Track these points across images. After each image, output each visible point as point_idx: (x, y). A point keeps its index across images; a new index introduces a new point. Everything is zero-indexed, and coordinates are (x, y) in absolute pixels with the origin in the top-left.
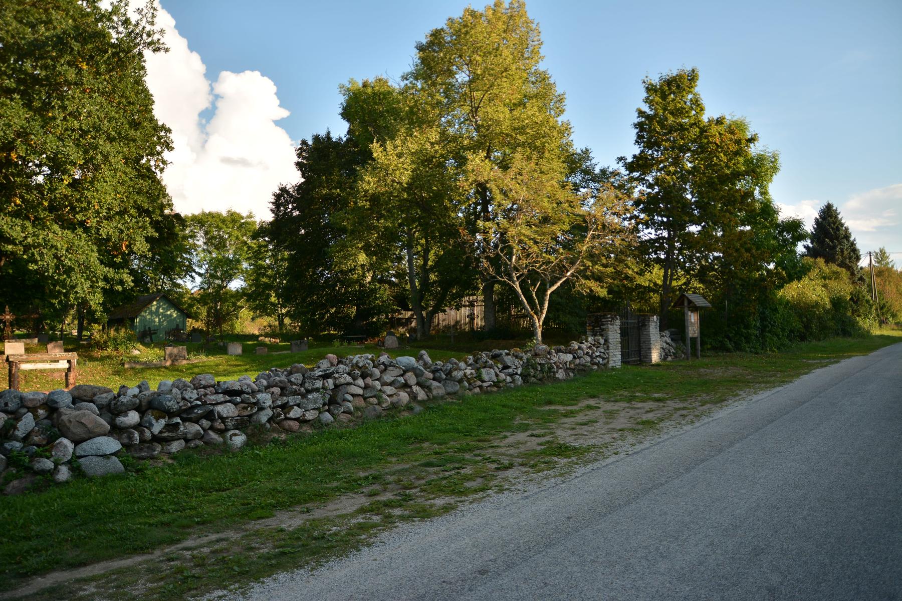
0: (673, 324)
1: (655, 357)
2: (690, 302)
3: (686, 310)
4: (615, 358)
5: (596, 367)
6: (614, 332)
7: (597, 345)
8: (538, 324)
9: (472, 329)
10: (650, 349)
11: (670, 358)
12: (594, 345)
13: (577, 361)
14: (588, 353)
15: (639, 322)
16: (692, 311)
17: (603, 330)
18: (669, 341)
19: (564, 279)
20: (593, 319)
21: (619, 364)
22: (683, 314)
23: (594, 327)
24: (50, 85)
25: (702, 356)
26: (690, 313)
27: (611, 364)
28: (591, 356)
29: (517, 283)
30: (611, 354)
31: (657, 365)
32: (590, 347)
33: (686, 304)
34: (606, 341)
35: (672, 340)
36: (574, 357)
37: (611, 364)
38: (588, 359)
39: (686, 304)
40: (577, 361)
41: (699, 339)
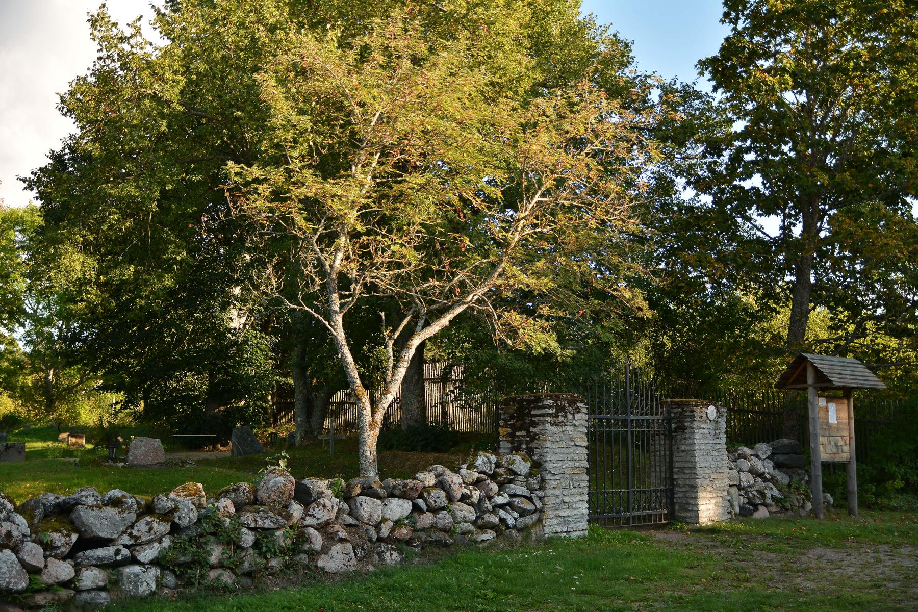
0: (771, 426)
1: (709, 509)
2: (820, 377)
3: (811, 393)
4: (569, 510)
5: (489, 535)
6: (566, 442)
7: (503, 478)
8: (368, 418)
9: (587, 447)
10: (694, 487)
11: (762, 513)
12: (493, 477)
13: (427, 519)
14: (464, 498)
15: (669, 421)
16: (830, 399)
17: (534, 437)
18: (766, 468)
19: (459, 310)
20: (513, 408)
21: (581, 528)
22: (805, 402)
23: (515, 429)
24: (866, 276)
25: (865, 505)
26: (822, 402)
27: (552, 526)
28: (478, 506)
29: (339, 319)
30: (551, 501)
31: (712, 531)
32: (477, 483)
33: (810, 380)
34: (537, 466)
35: (778, 466)
36: (416, 508)
37: (552, 526)
38: (471, 514)
39: (810, 380)
40: (427, 519)
41: (854, 467)
